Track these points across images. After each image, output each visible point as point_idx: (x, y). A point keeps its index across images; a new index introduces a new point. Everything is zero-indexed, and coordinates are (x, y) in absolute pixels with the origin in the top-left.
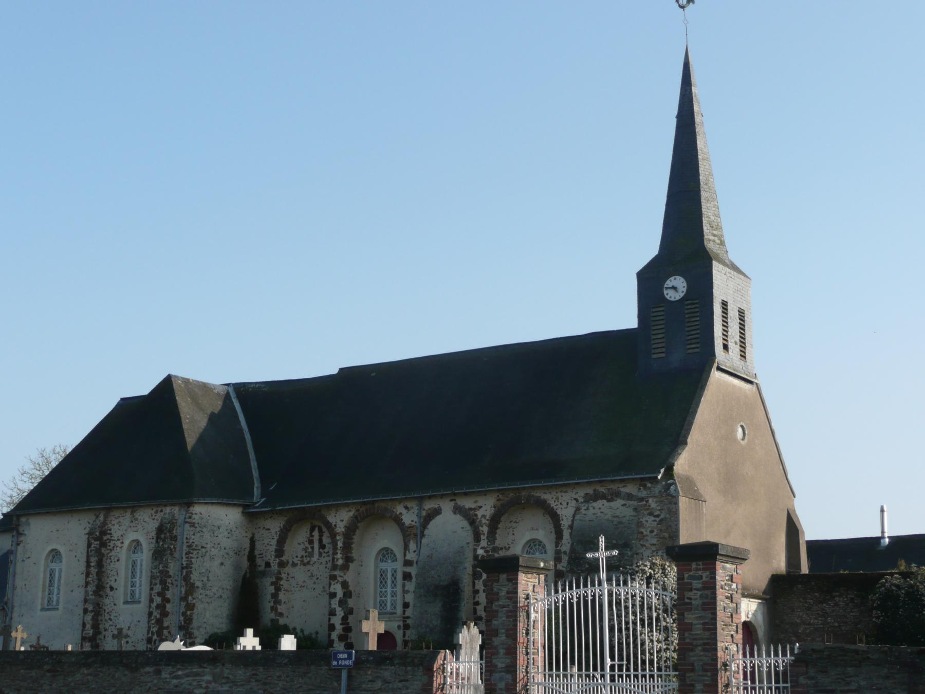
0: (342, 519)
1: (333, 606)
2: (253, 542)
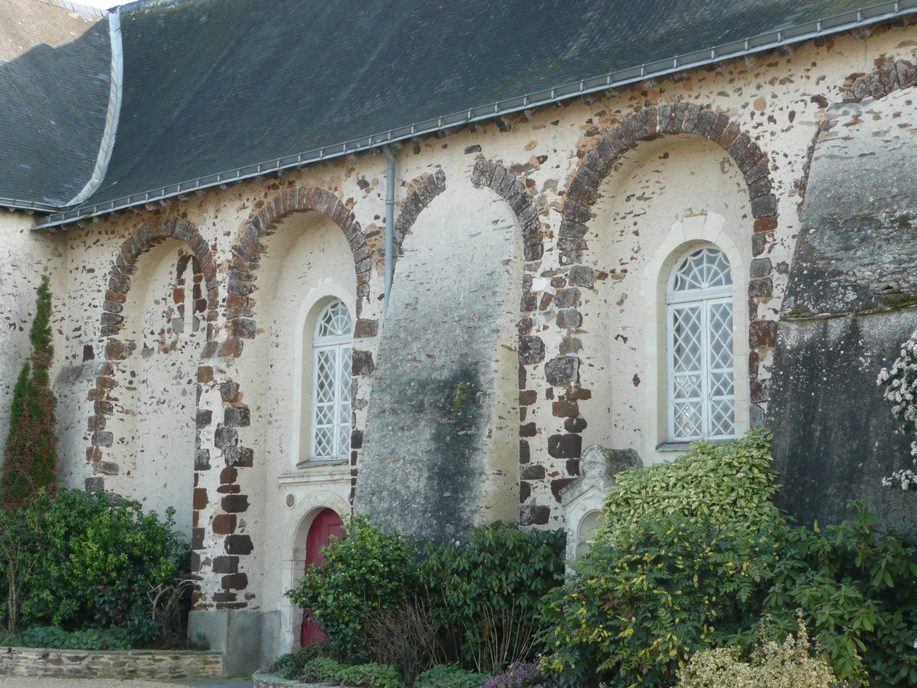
0: (227, 230)
1: (204, 446)
2: (44, 294)
